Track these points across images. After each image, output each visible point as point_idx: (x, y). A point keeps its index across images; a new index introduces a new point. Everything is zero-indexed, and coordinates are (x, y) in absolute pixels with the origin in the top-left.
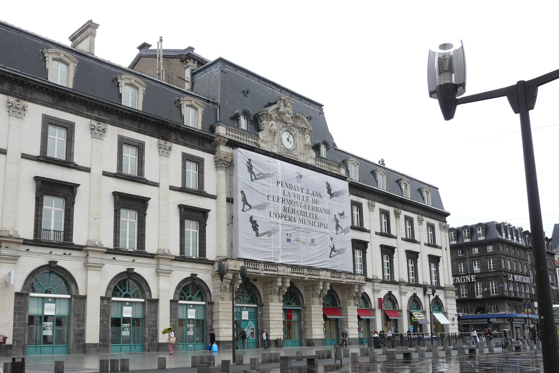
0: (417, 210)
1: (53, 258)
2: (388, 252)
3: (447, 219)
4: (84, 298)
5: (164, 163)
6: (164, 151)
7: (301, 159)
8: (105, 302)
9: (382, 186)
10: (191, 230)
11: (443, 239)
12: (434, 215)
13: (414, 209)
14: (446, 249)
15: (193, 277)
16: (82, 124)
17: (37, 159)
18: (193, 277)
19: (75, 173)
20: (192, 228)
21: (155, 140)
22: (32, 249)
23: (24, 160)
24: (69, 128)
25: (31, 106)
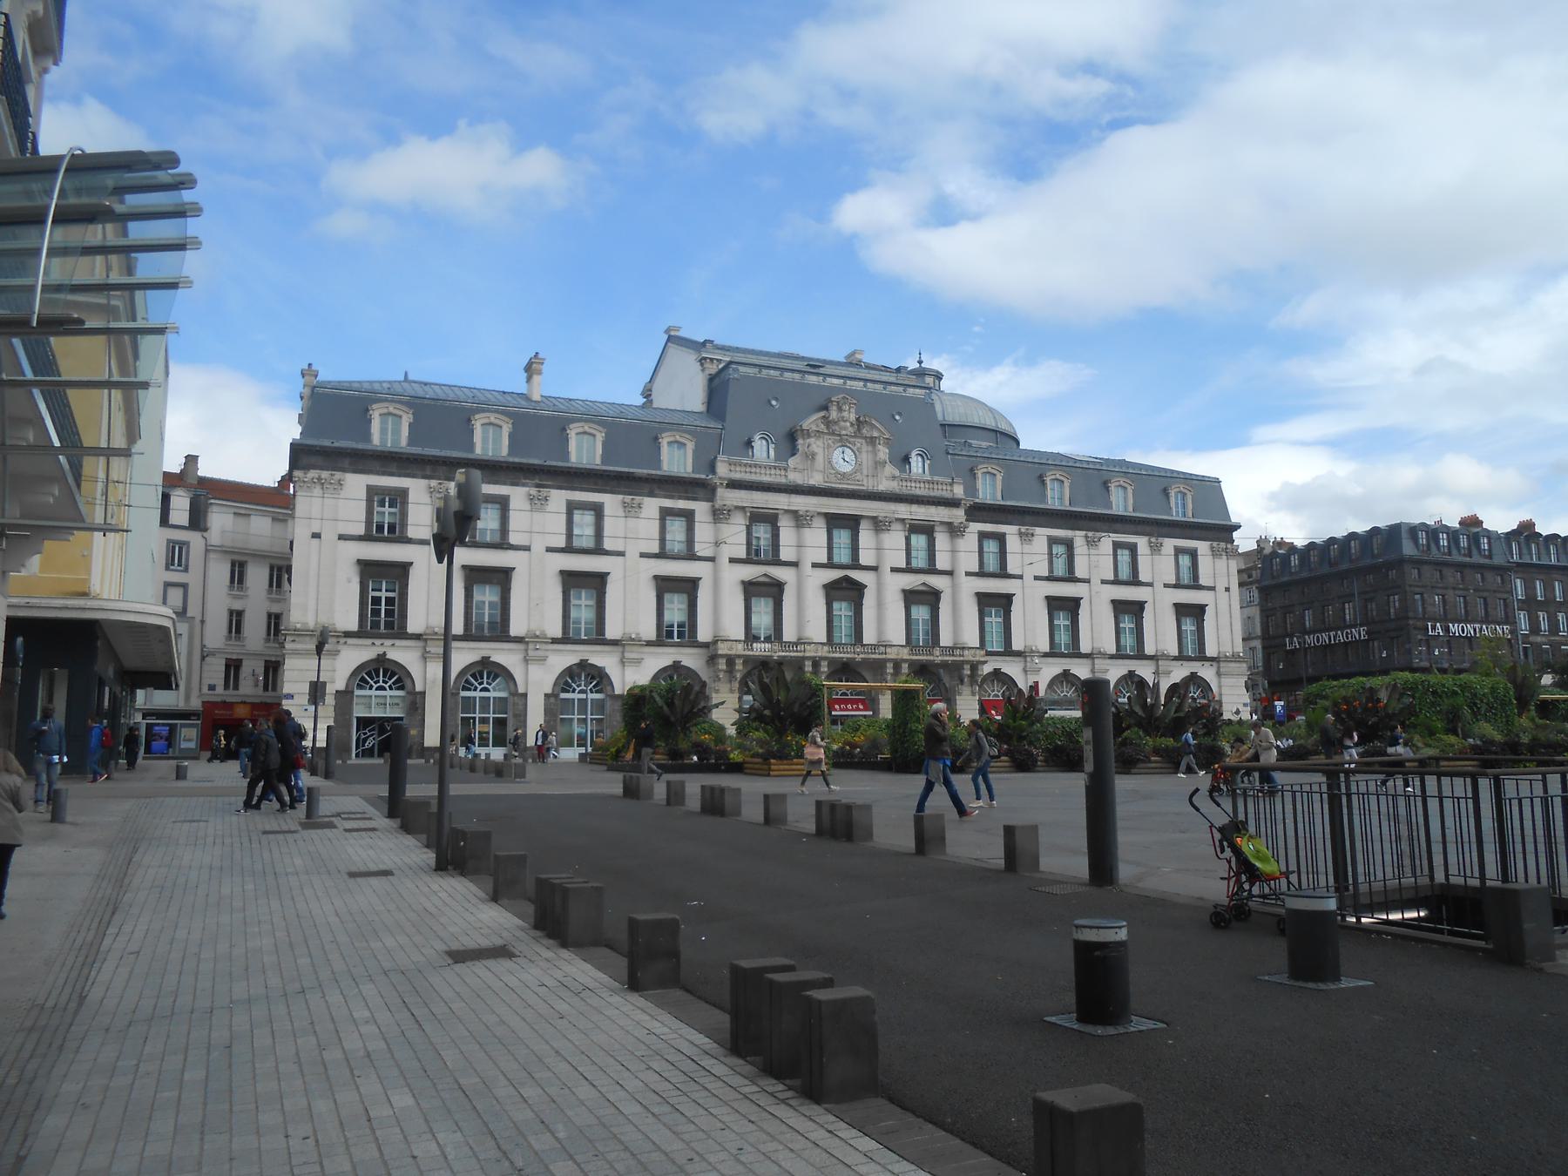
0: (1148, 529)
1: (485, 653)
2: (1129, 610)
3: (1235, 534)
4: (525, 695)
5: (633, 526)
6: (630, 510)
7: (869, 485)
8: (552, 700)
9: (1120, 502)
10: (843, 613)
11: (1219, 571)
12: (1196, 533)
13: (1140, 528)
14: (1227, 589)
16: (611, 502)
17: (1048, 579)
18: (1131, 674)
19: (511, 553)
20: (1062, 621)
21: (423, 482)
22: (1050, 660)
23: (342, 542)
24: (598, 510)
25: (1038, 530)
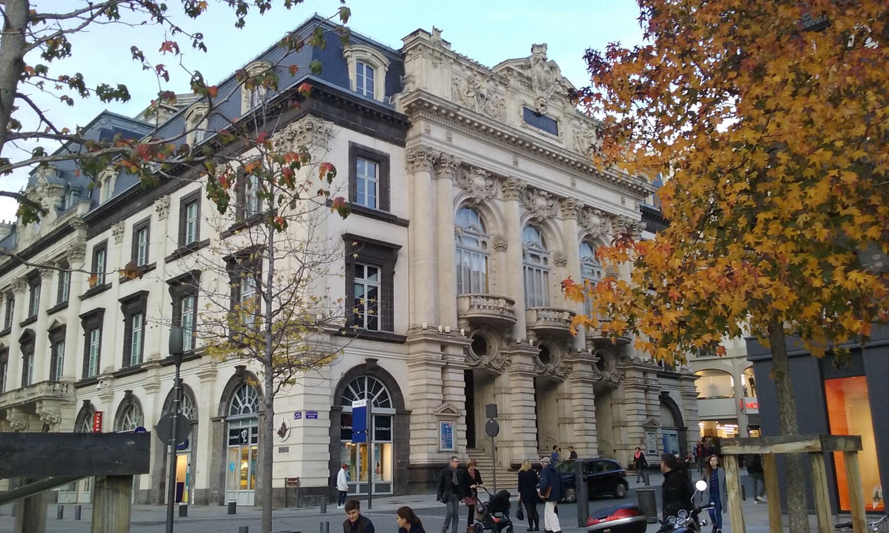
15: (372, 362)
18: (372, 362)
